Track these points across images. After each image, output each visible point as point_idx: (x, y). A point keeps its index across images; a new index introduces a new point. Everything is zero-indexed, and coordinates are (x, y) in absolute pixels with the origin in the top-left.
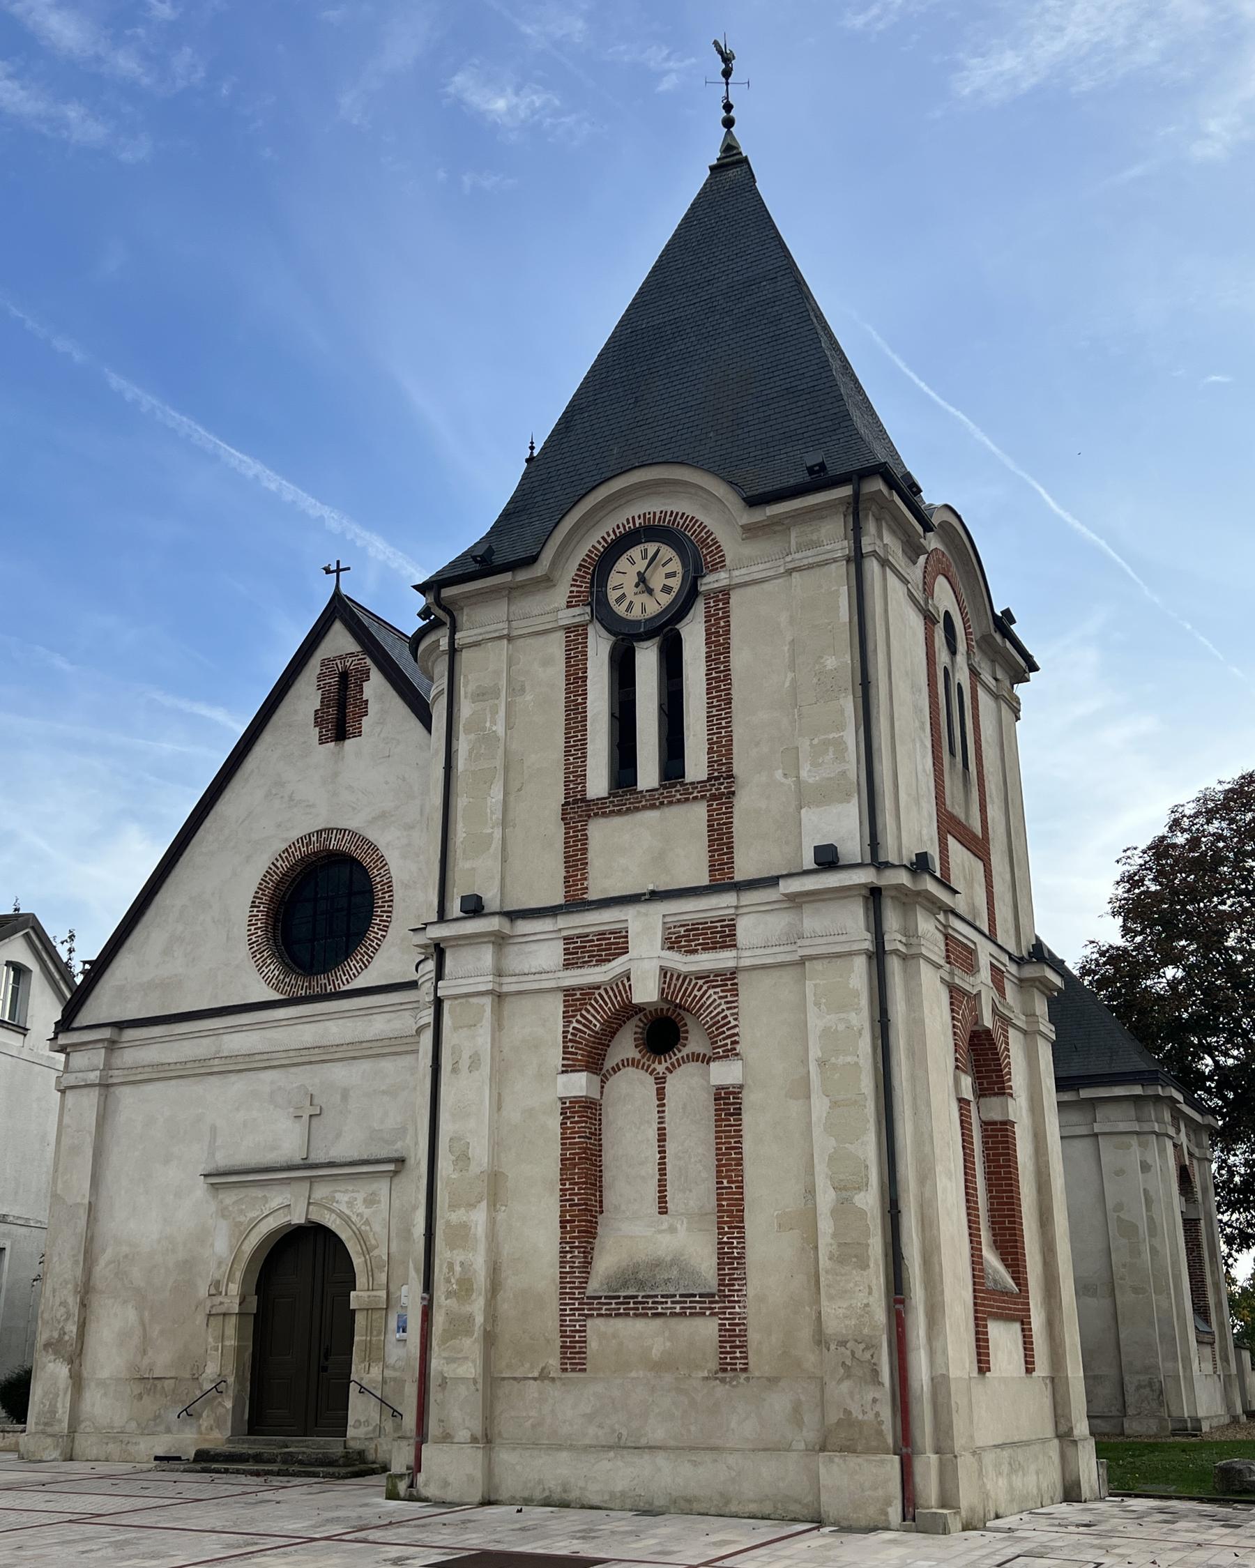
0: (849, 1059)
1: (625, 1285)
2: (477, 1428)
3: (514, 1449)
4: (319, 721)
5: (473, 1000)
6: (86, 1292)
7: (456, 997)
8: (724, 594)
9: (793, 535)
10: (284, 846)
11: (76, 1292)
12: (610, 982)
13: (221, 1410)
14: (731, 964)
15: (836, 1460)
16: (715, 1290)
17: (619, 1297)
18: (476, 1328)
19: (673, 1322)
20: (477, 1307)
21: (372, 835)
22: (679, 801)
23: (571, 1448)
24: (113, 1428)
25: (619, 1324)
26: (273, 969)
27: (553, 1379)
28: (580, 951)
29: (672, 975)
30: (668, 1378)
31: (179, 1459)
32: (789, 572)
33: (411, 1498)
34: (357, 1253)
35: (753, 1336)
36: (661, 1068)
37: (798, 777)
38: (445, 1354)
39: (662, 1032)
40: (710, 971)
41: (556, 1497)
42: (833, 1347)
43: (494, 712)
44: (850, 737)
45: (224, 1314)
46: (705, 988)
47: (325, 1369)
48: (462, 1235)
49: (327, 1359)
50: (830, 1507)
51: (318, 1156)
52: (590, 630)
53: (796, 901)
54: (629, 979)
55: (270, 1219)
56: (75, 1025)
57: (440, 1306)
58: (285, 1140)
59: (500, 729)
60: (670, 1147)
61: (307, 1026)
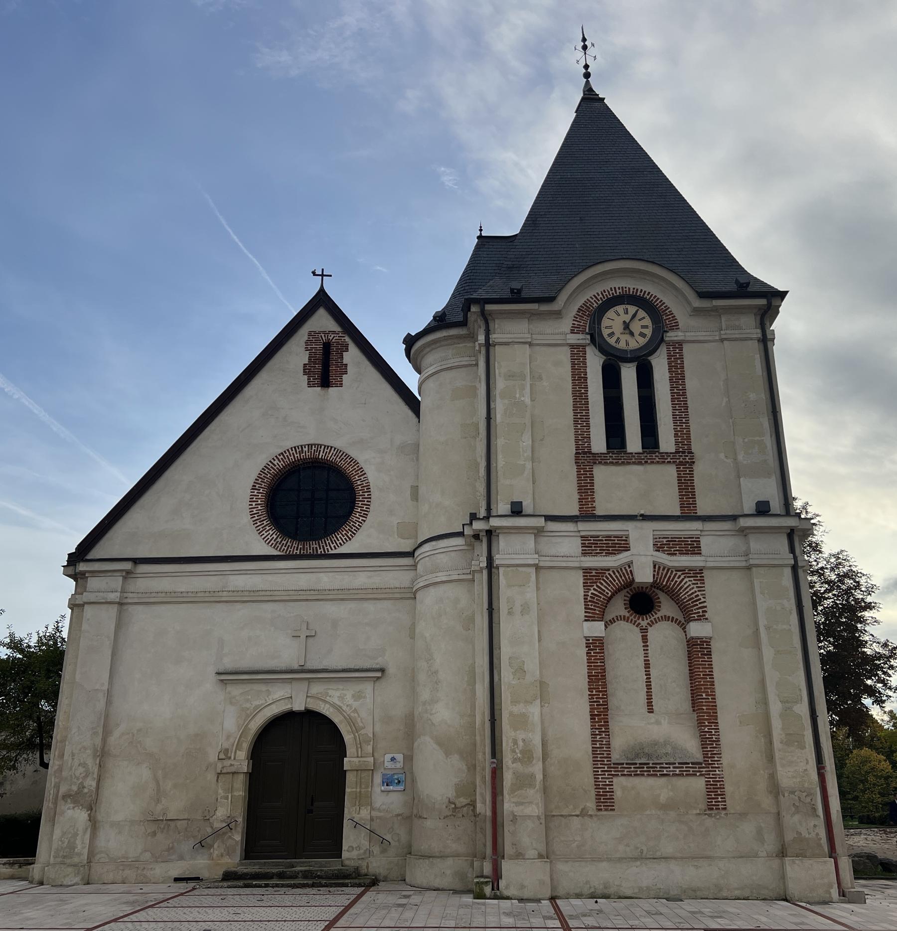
0: (785, 627)
1: (637, 756)
2: (542, 848)
3: (567, 862)
4: (307, 370)
5: (520, 569)
6: (102, 754)
7: (509, 566)
8: (679, 345)
9: (723, 319)
10: (280, 451)
11: (95, 756)
12: (616, 568)
13: (230, 842)
14: (702, 564)
15: (797, 862)
16: (701, 759)
17: (636, 764)
18: (538, 783)
19: (674, 780)
20: (537, 769)
21: (353, 453)
22: (658, 462)
23: (609, 860)
24: (127, 858)
25: (636, 781)
26: (272, 533)
27: (591, 816)
28: (591, 545)
29: (659, 567)
30: (673, 814)
31: (197, 879)
32: (722, 340)
33: (496, 897)
34: (348, 732)
35: (729, 788)
36: (644, 623)
37: (735, 459)
38: (515, 800)
39: (642, 602)
40: (687, 567)
41: (599, 892)
42: (786, 795)
43: (523, 388)
44: (769, 441)
45: (234, 773)
46: (682, 577)
47: (311, 811)
48: (522, 721)
49: (312, 805)
50: (794, 889)
51: (309, 666)
52: (588, 349)
53: (744, 532)
54: (629, 567)
55: (273, 706)
56: (89, 557)
57: (508, 768)
58: (287, 653)
59: (527, 400)
60: (653, 672)
61: (303, 575)
